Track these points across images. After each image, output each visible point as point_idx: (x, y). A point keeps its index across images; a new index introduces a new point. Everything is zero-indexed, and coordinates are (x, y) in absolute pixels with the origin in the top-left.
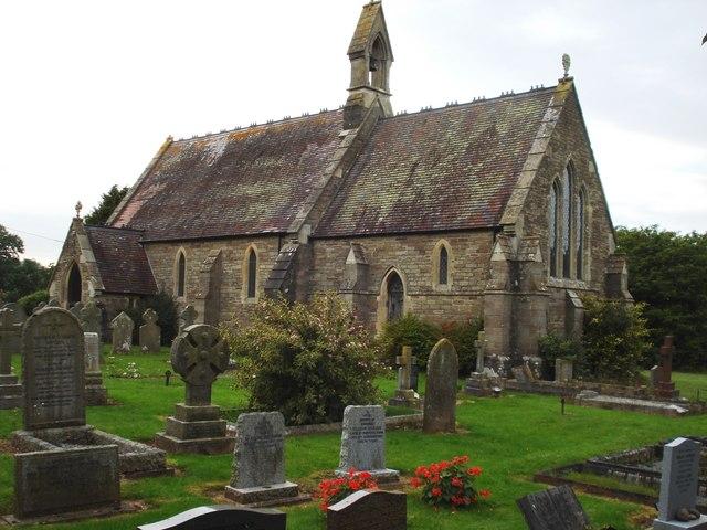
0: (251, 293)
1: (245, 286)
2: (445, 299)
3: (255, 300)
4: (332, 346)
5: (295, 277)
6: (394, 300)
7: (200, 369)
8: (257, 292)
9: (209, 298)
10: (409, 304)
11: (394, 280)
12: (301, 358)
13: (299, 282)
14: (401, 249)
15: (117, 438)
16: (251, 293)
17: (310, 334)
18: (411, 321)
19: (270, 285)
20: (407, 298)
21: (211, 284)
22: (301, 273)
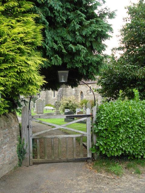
0: (54, 96)
1: (53, 95)
2: (91, 96)
3: (55, 98)
4: (73, 103)
5: (63, 93)
6: (82, 96)
7: (57, 106)
8: (55, 96)
9: (46, 97)
10: (85, 97)
11: (82, 92)
12: (69, 105)
13: (64, 94)
14: (82, 87)
15: (82, 132)
16: (54, 96)
17: (70, 101)
18: (85, 100)
19: (58, 94)
20: (84, 96)
21: (46, 95)
22: (64, 92)
